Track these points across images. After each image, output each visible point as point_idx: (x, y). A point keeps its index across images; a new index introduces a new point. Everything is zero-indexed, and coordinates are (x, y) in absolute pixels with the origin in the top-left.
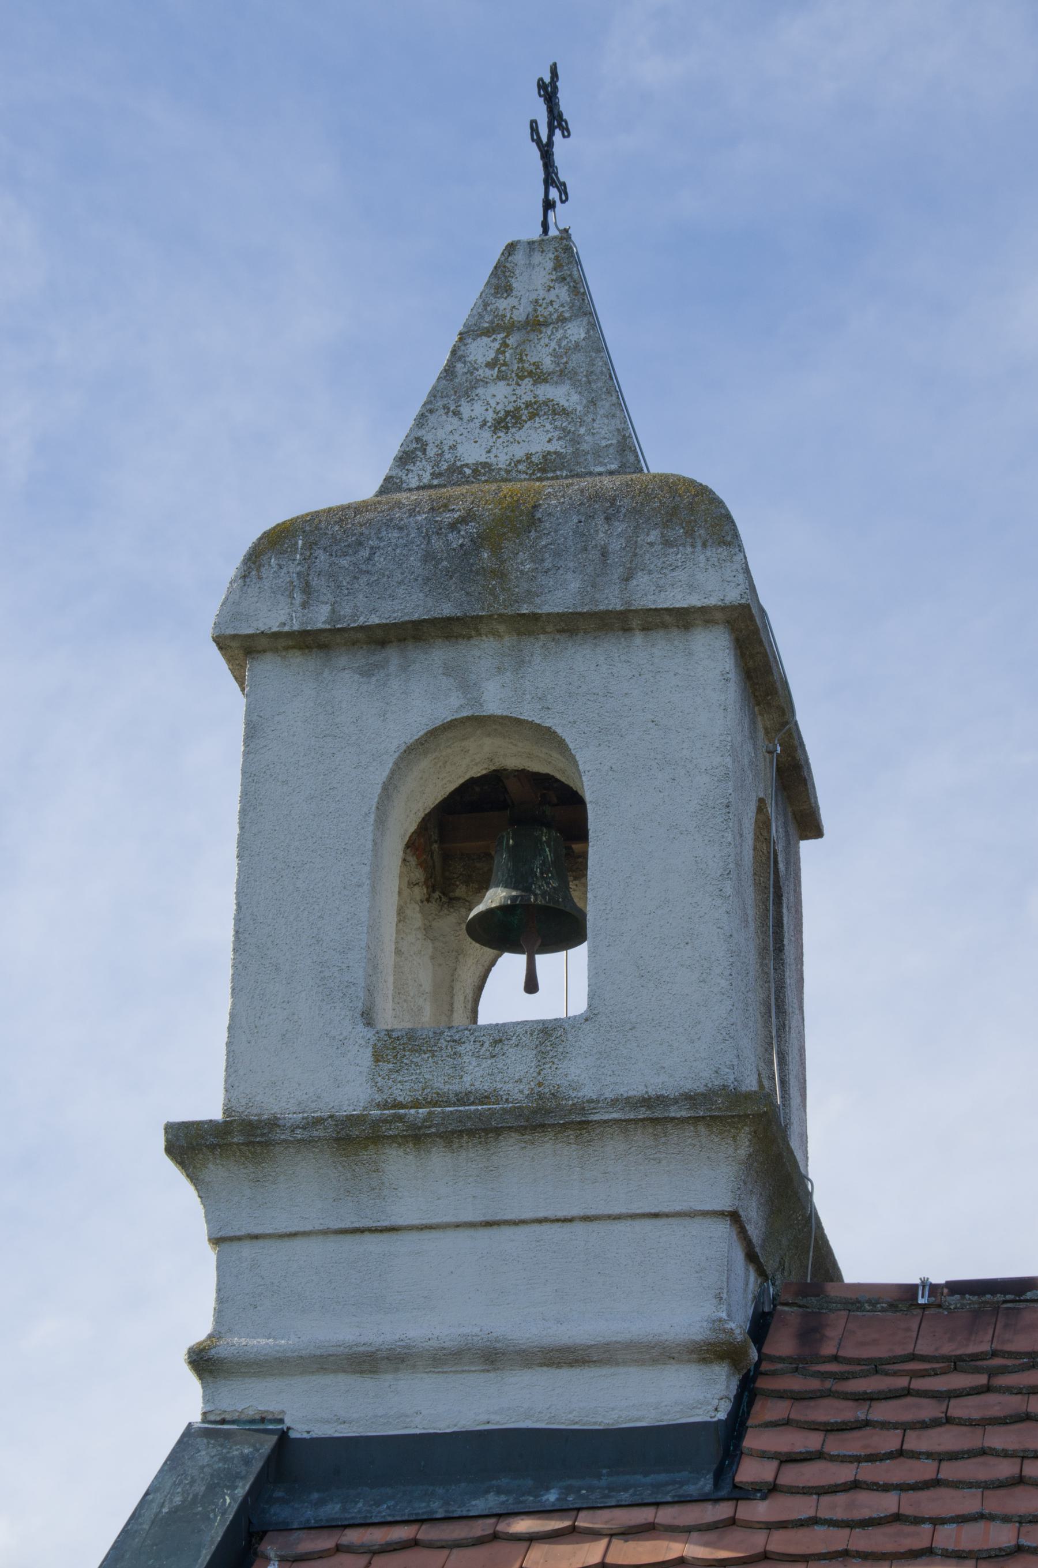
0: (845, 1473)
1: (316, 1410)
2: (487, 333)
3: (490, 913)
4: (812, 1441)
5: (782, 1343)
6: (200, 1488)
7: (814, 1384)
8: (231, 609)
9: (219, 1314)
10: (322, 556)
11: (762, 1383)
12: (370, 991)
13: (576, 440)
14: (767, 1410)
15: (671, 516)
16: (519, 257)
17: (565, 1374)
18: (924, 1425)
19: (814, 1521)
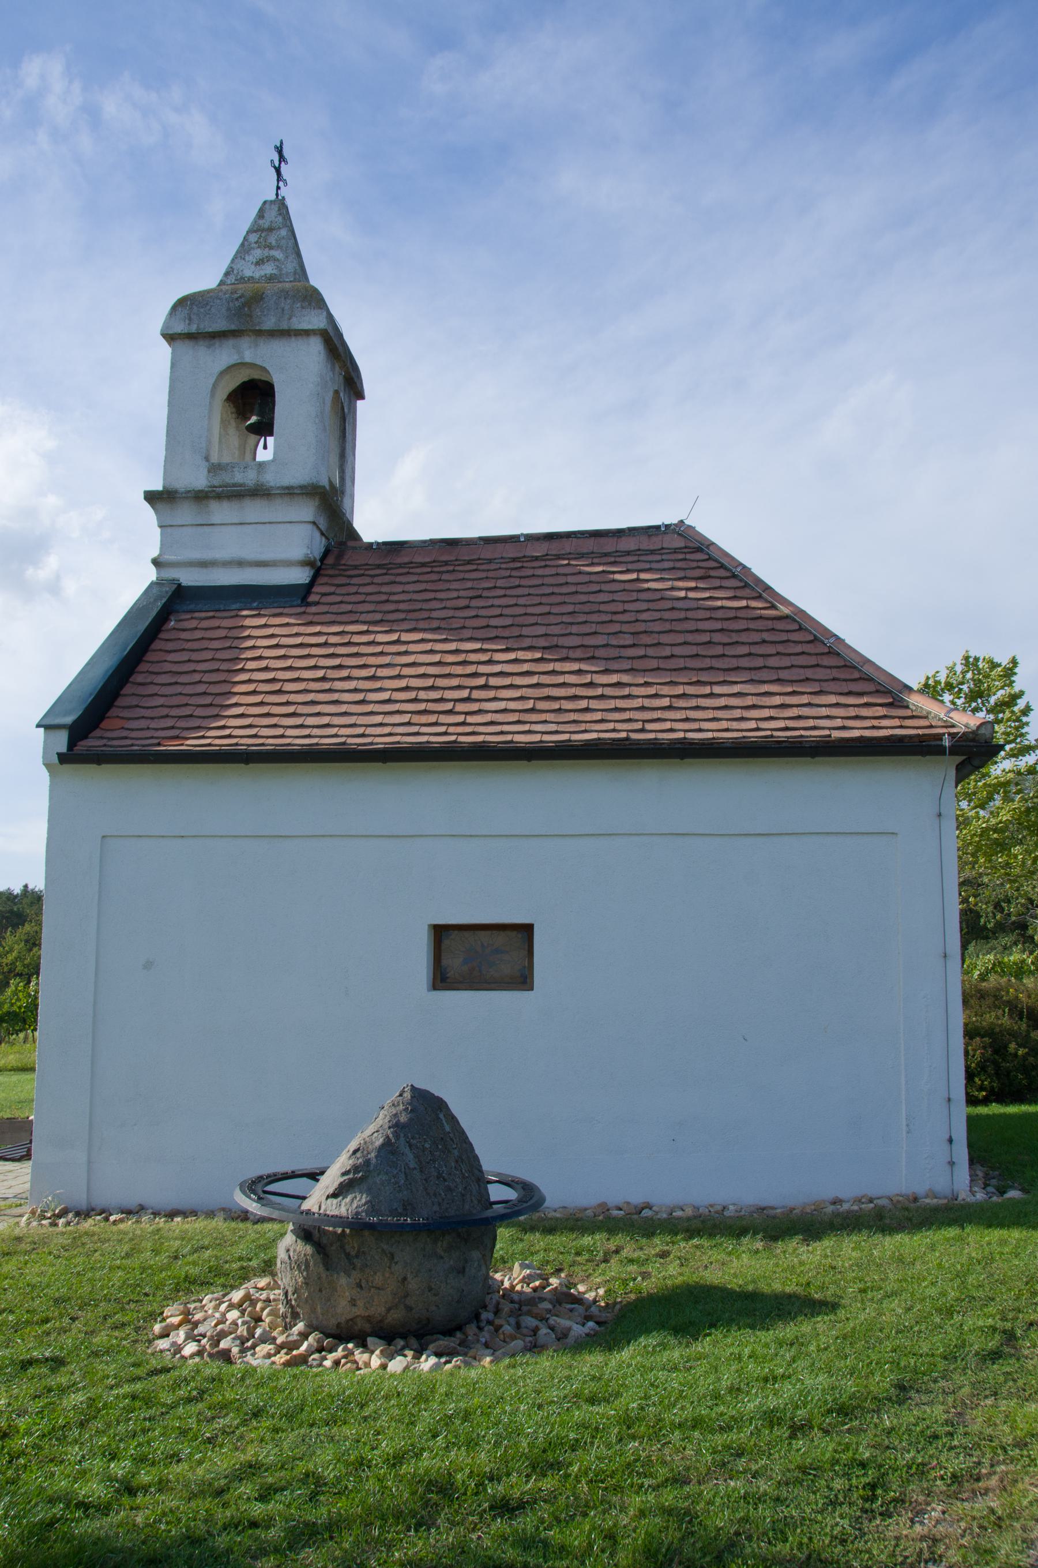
0: (339, 599)
1: (190, 578)
2: (255, 232)
3: (251, 424)
4: (332, 589)
5: (330, 560)
6: (152, 600)
7: (337, 572)
8: (166, 325)
9: (161, 549)
10: (195, 308)
11: (322, 572)
12: (208, 450)
13: (281, 270)
14: (322, 580)
15: (305, 298)
16: (267, 206)
17: (262, 569)
18: (365, 585)
19: (327, 613)
